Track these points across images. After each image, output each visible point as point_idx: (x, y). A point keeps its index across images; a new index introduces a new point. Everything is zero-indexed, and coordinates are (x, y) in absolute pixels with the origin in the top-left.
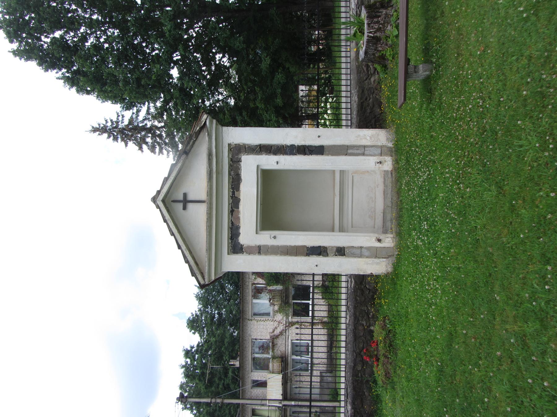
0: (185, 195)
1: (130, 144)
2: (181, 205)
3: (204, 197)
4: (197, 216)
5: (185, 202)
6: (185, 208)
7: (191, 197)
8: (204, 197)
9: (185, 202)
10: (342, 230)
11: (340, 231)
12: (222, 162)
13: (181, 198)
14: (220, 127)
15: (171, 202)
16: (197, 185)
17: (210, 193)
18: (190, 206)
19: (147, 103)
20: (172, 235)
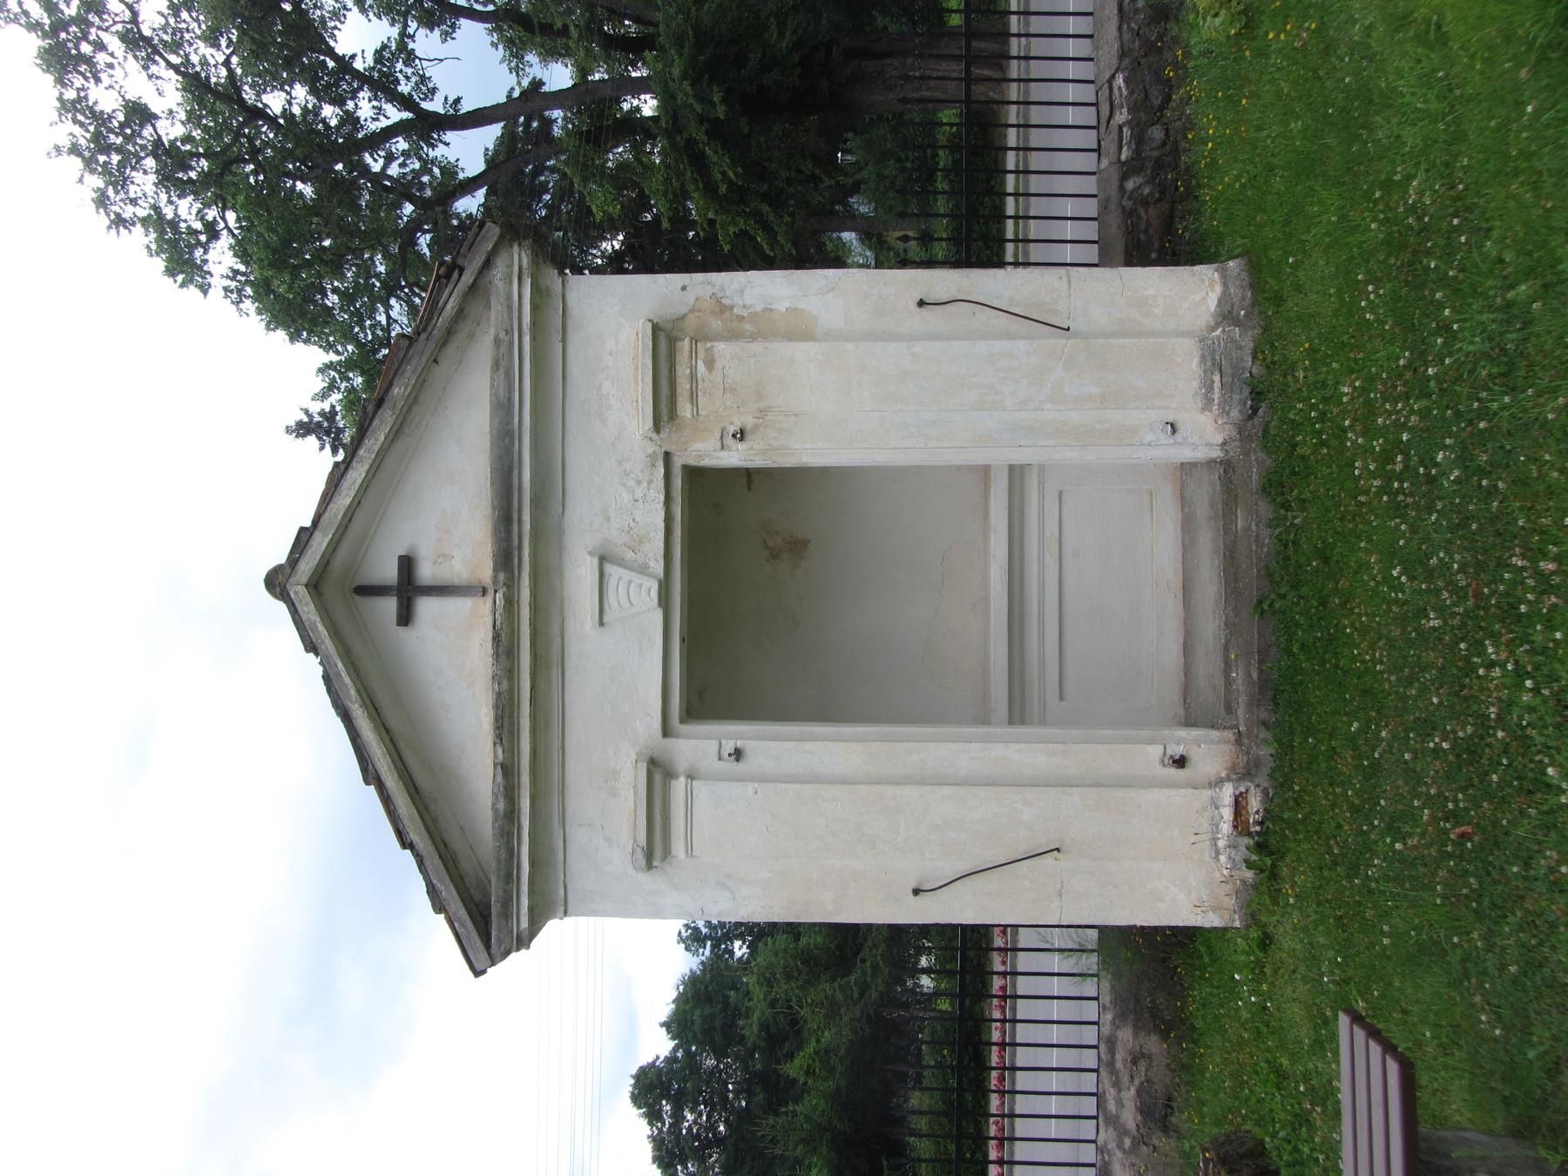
0: (407, 564)
1: (317, 460)
2: (390, 605)
3: (485, 571)
4: (452, 654)
5: (408, 588)
6: (405, 617)
7: (426, 572)
8: (715, 743)
9: (408, 588)
10: (1018, 713)
11: (1011, 722)
12: (1022, 585)
13: (388, 572)
14: (551, 276)
15: (340, 591)
16: (445, 515)
17: (505, 558)
18: (426, 607)
19: (296, 110)
20: (307, 651)
